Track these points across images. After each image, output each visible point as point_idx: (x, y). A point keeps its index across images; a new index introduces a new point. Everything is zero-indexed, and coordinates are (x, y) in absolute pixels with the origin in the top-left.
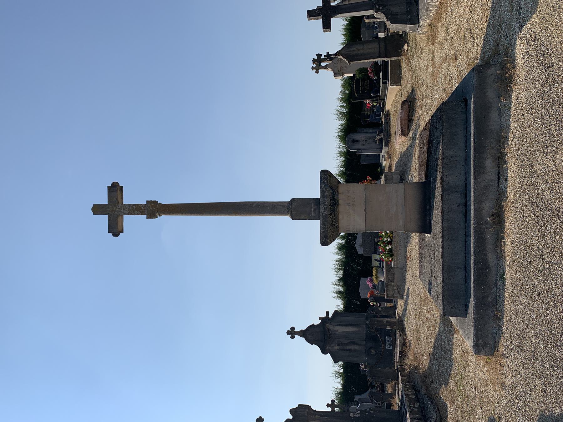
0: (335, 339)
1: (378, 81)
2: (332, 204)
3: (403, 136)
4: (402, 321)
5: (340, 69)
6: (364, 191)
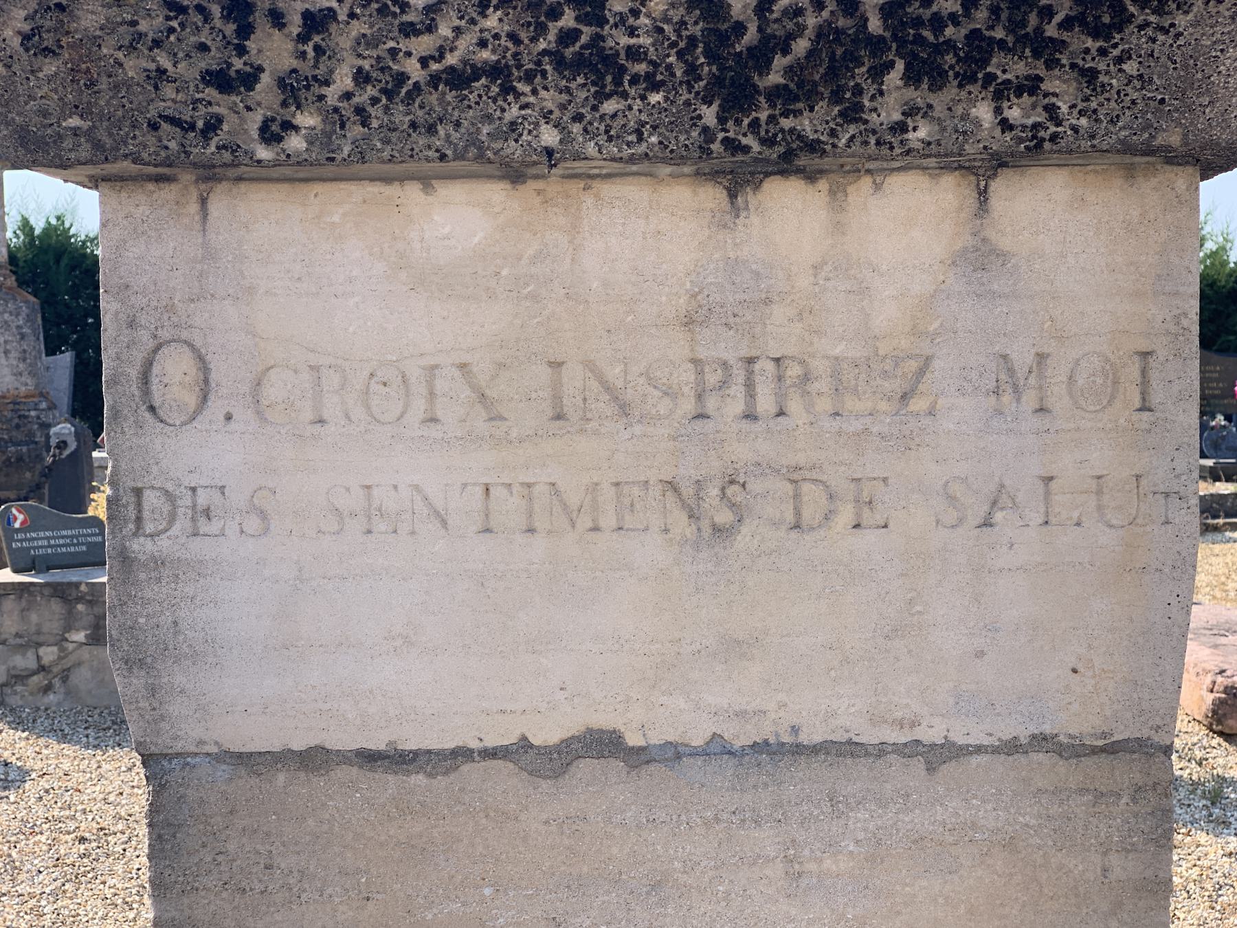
3: (1210, 698)
6: (1023, 733)
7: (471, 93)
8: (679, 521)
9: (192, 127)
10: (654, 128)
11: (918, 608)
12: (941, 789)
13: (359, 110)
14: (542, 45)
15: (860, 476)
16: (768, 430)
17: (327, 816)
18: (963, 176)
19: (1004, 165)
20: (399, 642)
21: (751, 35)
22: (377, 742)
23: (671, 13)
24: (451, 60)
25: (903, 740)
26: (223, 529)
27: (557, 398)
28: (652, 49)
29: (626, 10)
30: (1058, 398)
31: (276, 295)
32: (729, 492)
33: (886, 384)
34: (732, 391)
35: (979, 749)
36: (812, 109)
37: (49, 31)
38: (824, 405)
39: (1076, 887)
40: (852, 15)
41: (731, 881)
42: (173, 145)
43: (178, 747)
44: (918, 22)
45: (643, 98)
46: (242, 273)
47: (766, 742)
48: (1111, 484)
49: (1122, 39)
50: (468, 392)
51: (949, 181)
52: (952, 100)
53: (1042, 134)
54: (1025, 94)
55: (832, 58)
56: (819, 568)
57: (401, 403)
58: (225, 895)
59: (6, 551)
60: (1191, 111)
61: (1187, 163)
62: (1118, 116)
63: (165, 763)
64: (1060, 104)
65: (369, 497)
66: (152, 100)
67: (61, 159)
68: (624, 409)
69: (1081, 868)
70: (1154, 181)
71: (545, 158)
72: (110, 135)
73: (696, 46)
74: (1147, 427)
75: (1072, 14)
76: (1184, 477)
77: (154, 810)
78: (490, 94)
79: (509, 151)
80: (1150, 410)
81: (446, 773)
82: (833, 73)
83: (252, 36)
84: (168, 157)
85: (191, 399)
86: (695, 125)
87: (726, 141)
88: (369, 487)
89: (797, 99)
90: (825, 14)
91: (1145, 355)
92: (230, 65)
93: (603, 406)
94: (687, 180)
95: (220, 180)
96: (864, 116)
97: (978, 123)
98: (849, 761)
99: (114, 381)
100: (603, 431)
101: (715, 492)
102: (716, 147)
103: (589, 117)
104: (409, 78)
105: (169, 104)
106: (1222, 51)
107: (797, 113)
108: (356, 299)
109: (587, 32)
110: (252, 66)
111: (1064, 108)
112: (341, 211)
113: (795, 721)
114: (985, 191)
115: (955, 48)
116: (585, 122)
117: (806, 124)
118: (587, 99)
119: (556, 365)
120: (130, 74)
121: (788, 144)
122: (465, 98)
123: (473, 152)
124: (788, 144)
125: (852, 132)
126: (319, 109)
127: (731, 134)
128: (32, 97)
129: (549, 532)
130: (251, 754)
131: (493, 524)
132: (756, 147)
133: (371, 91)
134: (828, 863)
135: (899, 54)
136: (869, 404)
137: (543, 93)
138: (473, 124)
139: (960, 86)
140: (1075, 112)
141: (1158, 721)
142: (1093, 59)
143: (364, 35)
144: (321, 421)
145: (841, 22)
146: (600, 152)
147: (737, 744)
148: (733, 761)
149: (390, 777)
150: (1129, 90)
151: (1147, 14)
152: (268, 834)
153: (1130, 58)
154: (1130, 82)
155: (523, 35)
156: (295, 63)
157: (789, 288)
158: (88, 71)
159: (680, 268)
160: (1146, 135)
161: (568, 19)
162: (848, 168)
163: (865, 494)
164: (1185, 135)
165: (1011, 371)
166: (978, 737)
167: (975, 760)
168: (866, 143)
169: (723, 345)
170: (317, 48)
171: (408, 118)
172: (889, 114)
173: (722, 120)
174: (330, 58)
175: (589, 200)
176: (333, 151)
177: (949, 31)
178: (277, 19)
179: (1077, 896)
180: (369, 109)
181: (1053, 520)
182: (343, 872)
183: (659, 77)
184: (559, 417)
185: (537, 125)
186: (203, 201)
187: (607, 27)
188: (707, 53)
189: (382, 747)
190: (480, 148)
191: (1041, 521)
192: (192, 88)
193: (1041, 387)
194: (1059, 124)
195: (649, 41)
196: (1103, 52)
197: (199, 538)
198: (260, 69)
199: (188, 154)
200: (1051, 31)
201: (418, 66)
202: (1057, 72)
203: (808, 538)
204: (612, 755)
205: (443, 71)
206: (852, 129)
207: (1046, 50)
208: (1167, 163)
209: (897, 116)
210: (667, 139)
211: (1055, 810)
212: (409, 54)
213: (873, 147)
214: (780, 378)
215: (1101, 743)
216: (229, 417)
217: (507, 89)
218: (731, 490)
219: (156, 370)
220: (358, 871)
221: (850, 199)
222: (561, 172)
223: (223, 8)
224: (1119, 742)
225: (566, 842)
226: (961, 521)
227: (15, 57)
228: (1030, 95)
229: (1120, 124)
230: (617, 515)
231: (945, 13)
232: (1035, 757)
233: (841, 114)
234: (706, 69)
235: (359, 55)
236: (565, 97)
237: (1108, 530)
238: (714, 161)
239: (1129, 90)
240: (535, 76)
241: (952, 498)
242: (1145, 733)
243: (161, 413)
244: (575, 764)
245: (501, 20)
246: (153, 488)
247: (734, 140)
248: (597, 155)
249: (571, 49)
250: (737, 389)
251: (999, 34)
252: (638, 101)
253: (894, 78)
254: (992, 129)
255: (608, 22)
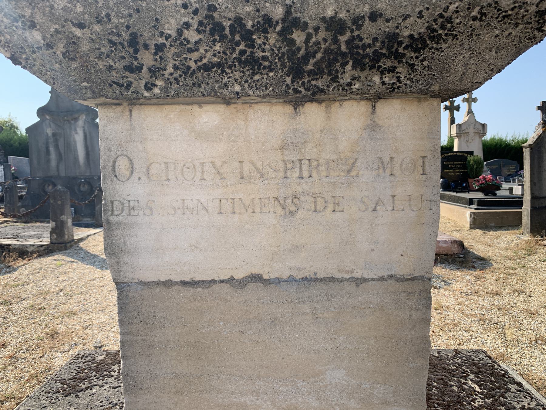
0: (64, 129)
1: (467, 189)
2: (298, 37)
4: (66, 249)
5: (466, 133)
6: (386, 274)
7: (211, 73)
8: (279, 210)
9: (123, 85)
10: (271, 85)
11: (353, 236)
12: (360, 292)
13: (176, 79)
14: (234, 56)
15: (334, 196)
16: (307, 182)
17: (172, 301)
18: (367, 101)
19: (380, 98)
20: (193, 248)
21: (303, 52)
22: (187, 278)
23: (276, 44)
24: (205, 61)
25: (349, 277)
26: (138, 213)
27: (241, 172)
28: (270, 57)
29: (261, 43)
30: (397, 171)
31: (153, 140)
32: (294, 201)
33: (343, 167)
34: (295, 170)
35: (372, 280)
36: (322, 78)
37: (72, 52)
38: (324, 174)
39: (401, 321)
40: (336, 44)
41: (296, 320)
42: (117, 92)
43: (126, 280)
44: (358, 47)
45: (267, 74)
46: (143, 134)
47: (306, 278)
48: (413, 198)
49: (424, 53)
50: (214, 171)
51: (363, 103)
52: (367, 75)
53: (395, 86)
54: (391, 73)
55: (329, 59)
56: (322, 224)
57: (193, 175)
58: (141, 325)
59: (449, 163)
60: (443, 78)
61: (437, 97)
62: (419, 80)
63: (122, 285)
64: (401, 76)
65: (184, 203)
66: (109, 76)
67: (82, 97)
68: (262, 176)
69: (403, 315)
70: (427, 103)
71: (236, 96)
72: (97, 88)
73: (285, 56)
74: (425, 180)
75: (408, 44)
76: (436, 195)
77: (119, 299)
78: (218, 73)
79: (225, 93)
80: (425, 174)
81: (208, 287)
82: (329, 65)
83: (139, 53)
84: (116, 96)
85: (128, 173)
86: (284, 84)
87: (294, 89)
88: (183, 200)
89: (317, 74)
90: (327, 44)
91: (424, 157)
92: (133, 64)
93: (256, 175)
94: (281, 104)
95: (136, 105)
96: (339, 80)
97: (375, 82)
98: (332, 283)
99: (104, 168)
100: (256, 182)
101: (290, 201)
102: (291, 91)
103: (250, 81)
104: (191, 68)
105: (115, 77)
106: (456, 57)
107: (317, 79)
108: (178, 142)
109: (249, 50)
110: (140, 64)
111: (403, 78)
112: (173, 114)
113: (316, 271)
114: (374, 106)
115: (369, 56)
116: (249, 83)
117: (319, 84)
118: (249, 75)
119: (241, 162)
120: (101, 67)
121: (314, 90)
122: (210, 75)
123: (213, 93)
124: (314, 90)
125: (334, 86)
126: (163, 79)
127: (295, 87)
128: (70, 76)
129: (240, 213)
130: (148, 282)
131: (222, 211)
132: (303, 91)
133: (179, 73)
134: (326, 314)
135: (351, 59)
136: (338, 174)
137: (235, 73)
138: (213, 84)
139: (370, 69)
140: (406, 79)
141: (427, 270)
142: (414, 60)
143: (175, 53)
144: (168, 180)
145: (333, 47)
146: (254, 93)
147: (298, 278)
148: (296, 283)
149: (191, 289)
150: (424, 71)
151: (433, 44)
152: (154, 307)
153: (425, 60)
154: (425, 68)
155: (228, 52)
156: (154, 63)
157: (313, 138)
158: (87, 66)
159: (279, 131)
160: (428, 87)
161: (242, 47)
162: (331, 99)
163: (336, 201)
164: (440, 87)
165: (382, 163)
166: (372, 276)
167: (371, 283)
168: (339, 89)
169: (292, 156)
170: (160, 57)
171: (192, 82)
172: (346, 80)
173: (293, 82)
174: (165, 61)
175: (251, 111)
176: (168, 93)
177: (368, 50)
178: (146, 47)
179: (402, 324)
180: (179, 79)
181: (395, 209)
182: (177, 318)
183: (272, 67)
184: (242, 178)
185: (233, 84)
186: (130, 111)
187: (255, 49)
188: (288, 58)
189: (189, 280)
190: (215, 92)
191: (391, 209)
192: (121, 72)
193: (392, 168)
194: (400, 83)
195: (269, 54)
196: (417, 58)
197: (131, 216)
198: (143, 65)
199: (123, 95)
200: (401, 50)
201: (194, 63)
202: (401, 65)
203: (319, 215)
204: (259, 281)
205: (202, 65)
206: (334, 85)
207: (398, 57)
208: (431, 97)
209: (349, 80)
210: (275, 89)
211: (396, 298)
212: (191, 59)
213: (341, 91)
214: (310, 166)
215: (409, 277)
216: (139, 179)
217: (223, 71)
218: (295, 200)
219: (117, 164)
220: (182, 317)
221: (332, 109)
222: (241, 101)
223: (128, 43)
224: (415, 277)
225: (245, 308)
226: (366, 209)
227: (62, 61)
228: (392, 73)
229: (420, 83)
230: (260, 208)
231: (366, 44)
232: (390, 282)
233: (331, 79)
234: (288, 64)
235: (174, 60)
236: (242, 74)
237: (412, 212)
238: (290, 97)
239: (424, 71)
240: (232, 67)
241: (364, 202)
242: (423, 274)
243: (118, 177)
244: (248, 284)
245: (220, 47)
246: (116, 201)
247: (297, 89)
248: (252, 94)
249: (244, 57)
250: (297, 170)
251: (384, 51)
252: (266, 75)
253: (349, 67)
254: (379, 85)
255: (256, 47)
